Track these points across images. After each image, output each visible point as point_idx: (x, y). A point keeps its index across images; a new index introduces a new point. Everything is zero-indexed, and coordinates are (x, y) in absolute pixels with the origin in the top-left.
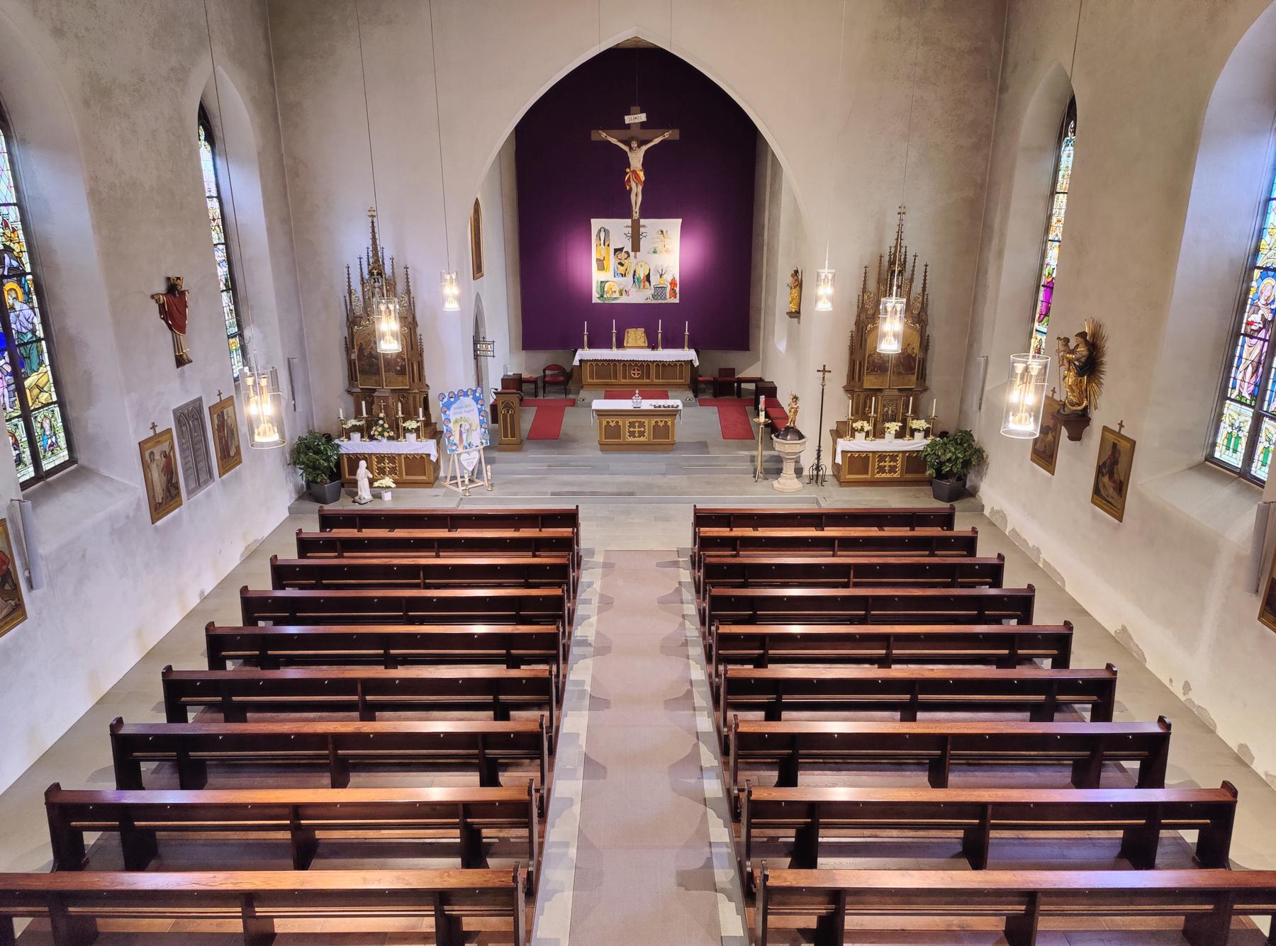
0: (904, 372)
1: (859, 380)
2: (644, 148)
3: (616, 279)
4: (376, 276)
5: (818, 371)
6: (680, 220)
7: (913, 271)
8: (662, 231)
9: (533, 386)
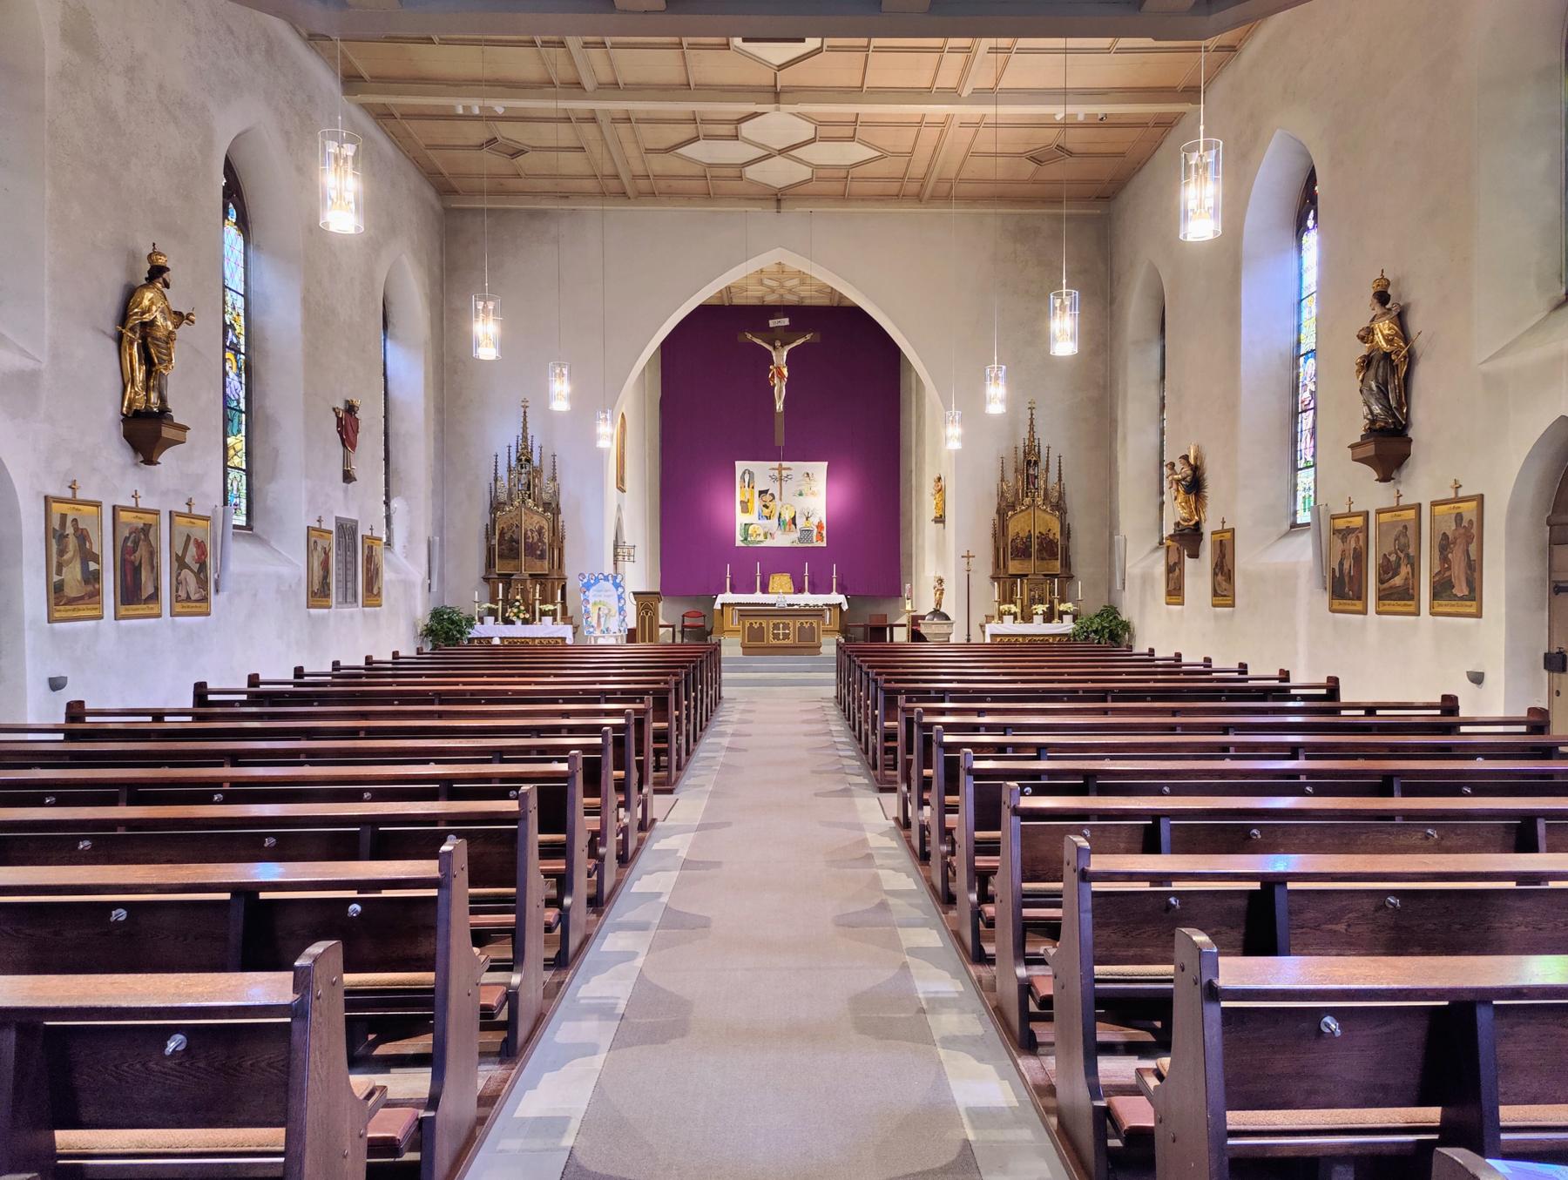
0: (1047, 557)
1: (1004, 567)
2: (788, 348)
3: (760, 522)
4: (523, 462)
5: (963, 557)
6: (827, 463)
7: (1048, 461)
8: (808, 474)
9: (671, 629)
